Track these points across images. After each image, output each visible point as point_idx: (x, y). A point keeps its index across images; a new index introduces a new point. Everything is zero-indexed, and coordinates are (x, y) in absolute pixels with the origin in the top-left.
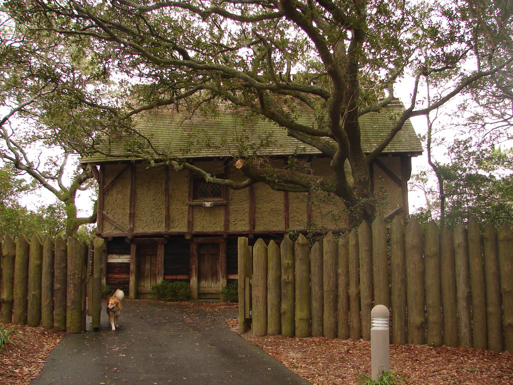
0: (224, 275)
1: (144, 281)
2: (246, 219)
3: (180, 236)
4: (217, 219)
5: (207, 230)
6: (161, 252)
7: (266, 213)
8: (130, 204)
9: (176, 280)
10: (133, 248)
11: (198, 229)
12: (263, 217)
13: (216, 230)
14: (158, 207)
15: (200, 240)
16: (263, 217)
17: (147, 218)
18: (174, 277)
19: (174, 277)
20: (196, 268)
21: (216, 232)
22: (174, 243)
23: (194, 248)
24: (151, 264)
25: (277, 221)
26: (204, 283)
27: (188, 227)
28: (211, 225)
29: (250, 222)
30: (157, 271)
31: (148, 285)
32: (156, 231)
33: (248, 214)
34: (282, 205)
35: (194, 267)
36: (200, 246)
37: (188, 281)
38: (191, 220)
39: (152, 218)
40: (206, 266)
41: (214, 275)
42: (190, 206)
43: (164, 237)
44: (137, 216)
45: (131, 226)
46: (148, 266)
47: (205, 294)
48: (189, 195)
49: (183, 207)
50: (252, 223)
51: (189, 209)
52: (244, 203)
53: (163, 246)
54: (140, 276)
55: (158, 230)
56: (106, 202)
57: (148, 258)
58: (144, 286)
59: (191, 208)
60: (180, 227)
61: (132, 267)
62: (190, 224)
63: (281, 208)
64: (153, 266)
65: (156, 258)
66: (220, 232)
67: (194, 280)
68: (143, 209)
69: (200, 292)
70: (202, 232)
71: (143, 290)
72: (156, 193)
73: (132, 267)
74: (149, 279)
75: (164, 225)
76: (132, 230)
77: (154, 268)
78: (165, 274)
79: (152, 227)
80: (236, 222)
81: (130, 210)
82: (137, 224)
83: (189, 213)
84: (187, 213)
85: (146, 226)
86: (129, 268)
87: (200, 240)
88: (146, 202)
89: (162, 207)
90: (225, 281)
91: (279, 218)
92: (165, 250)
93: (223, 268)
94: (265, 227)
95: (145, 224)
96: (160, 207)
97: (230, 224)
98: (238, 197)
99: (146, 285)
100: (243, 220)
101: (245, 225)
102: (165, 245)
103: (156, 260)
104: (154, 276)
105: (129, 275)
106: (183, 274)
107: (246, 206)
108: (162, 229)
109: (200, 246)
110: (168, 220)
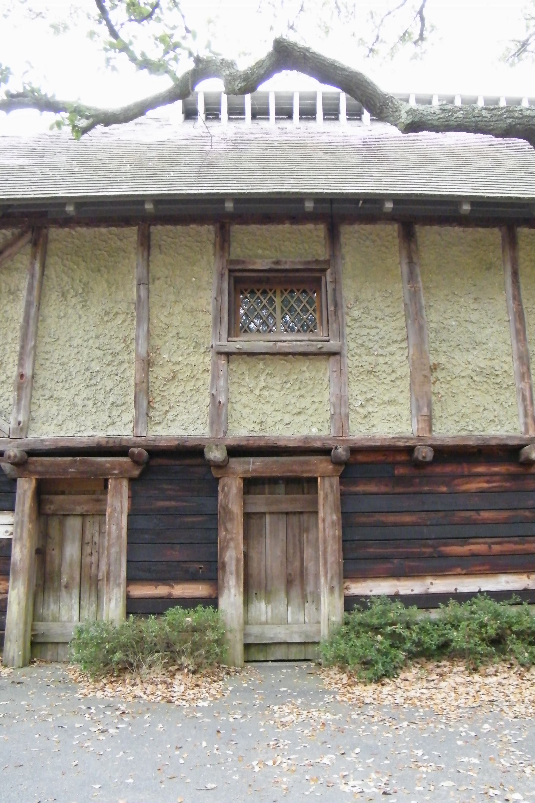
0: (335, 583)
1: (58, 600)
2: (401, 399)
3: (189, 453)
4: (309, 400)
5: (277, 434)
6: (118, 503)
7: (463, 381)
8: (22, 347)
9: (169, 602)
10: (25, 488)
11: (244, 428)
12: (454, 395)
13: (304, 432)
14: (110, 358)
15: (254, 465)
16: (454, 395)
17: (73, 391)
18: (162, 590)
19: (162, 590)
20: (238, 560)
21: (306, 439)
22: (172, 478)
23: (231, 491)
24: (83, 543)
25: (496, 406)
26: (261, 609)
27: (212, 424)
28: (287, 418)
29: (419, 409)
30: (103, 568)
31: (68, 614)
32: (102, 434)
33: (407, 382)
34: (509, 359)
35: (232, 556)
36: (251, 484)
37: (212, 602)
38: (222, 399)
39: (90, 395)
40: (271, 552)
41: (296, 581)
42: (220, 353)
43: (132, 456)
44: (43, 387)
45: (21, 418)
46: (72, 551)
47: (265, 646)
48: (217, 321)
49: (193, 359)
50: (425, 411)
51: (215, 365)
52: (394, 348)
53: (125, 484)
54: (45, 580)
55: (112, 432)
56: (280, 516)
57: (74, 524)
58: (56, 619)
59: (223, 361)
60: (182, 422)
61: (20, 554)
62: (218, 411)
63: (506, 367)
64: (88, 549)
65: (102, 524)
66: (320, 439)
67: (231, 599)
68: (62, 364)
69: (250, 641)
70: (260, 438)
71: (51, 629)
72: (107, 313)
73: (20, 554)
74: (75, 592)
75: (129, 416)
76: (22, 428)
77: (94, 559)
78: (131, 580)
79: (89, 423)
80: (370, 409)
81: (21, 364)
82: (42, 412)
83: (215, 378)
84: (208, 377)
85: (70, 418)
86: (8, 557)
87: (254, 465)
88: (75, 342)
89: (125, 357)
90: (340, 604)
91: (502, 398)
92: (132, 497)
93: (331, 559)
94: (463, 423)
95: (66, 412)
96: (120, 358)
97: (352, 416)
98: (373, 332)
99: (64, 616)
100: (391, 402)
101: (398, 417)
102: (132, 481)
103: (101, 533)
104: (91, 583)
105: (8, 580)
106: (193, 578)
107: (400, 361)
108: (122, 428)
109: (251, 484)
110: (145, 397)
